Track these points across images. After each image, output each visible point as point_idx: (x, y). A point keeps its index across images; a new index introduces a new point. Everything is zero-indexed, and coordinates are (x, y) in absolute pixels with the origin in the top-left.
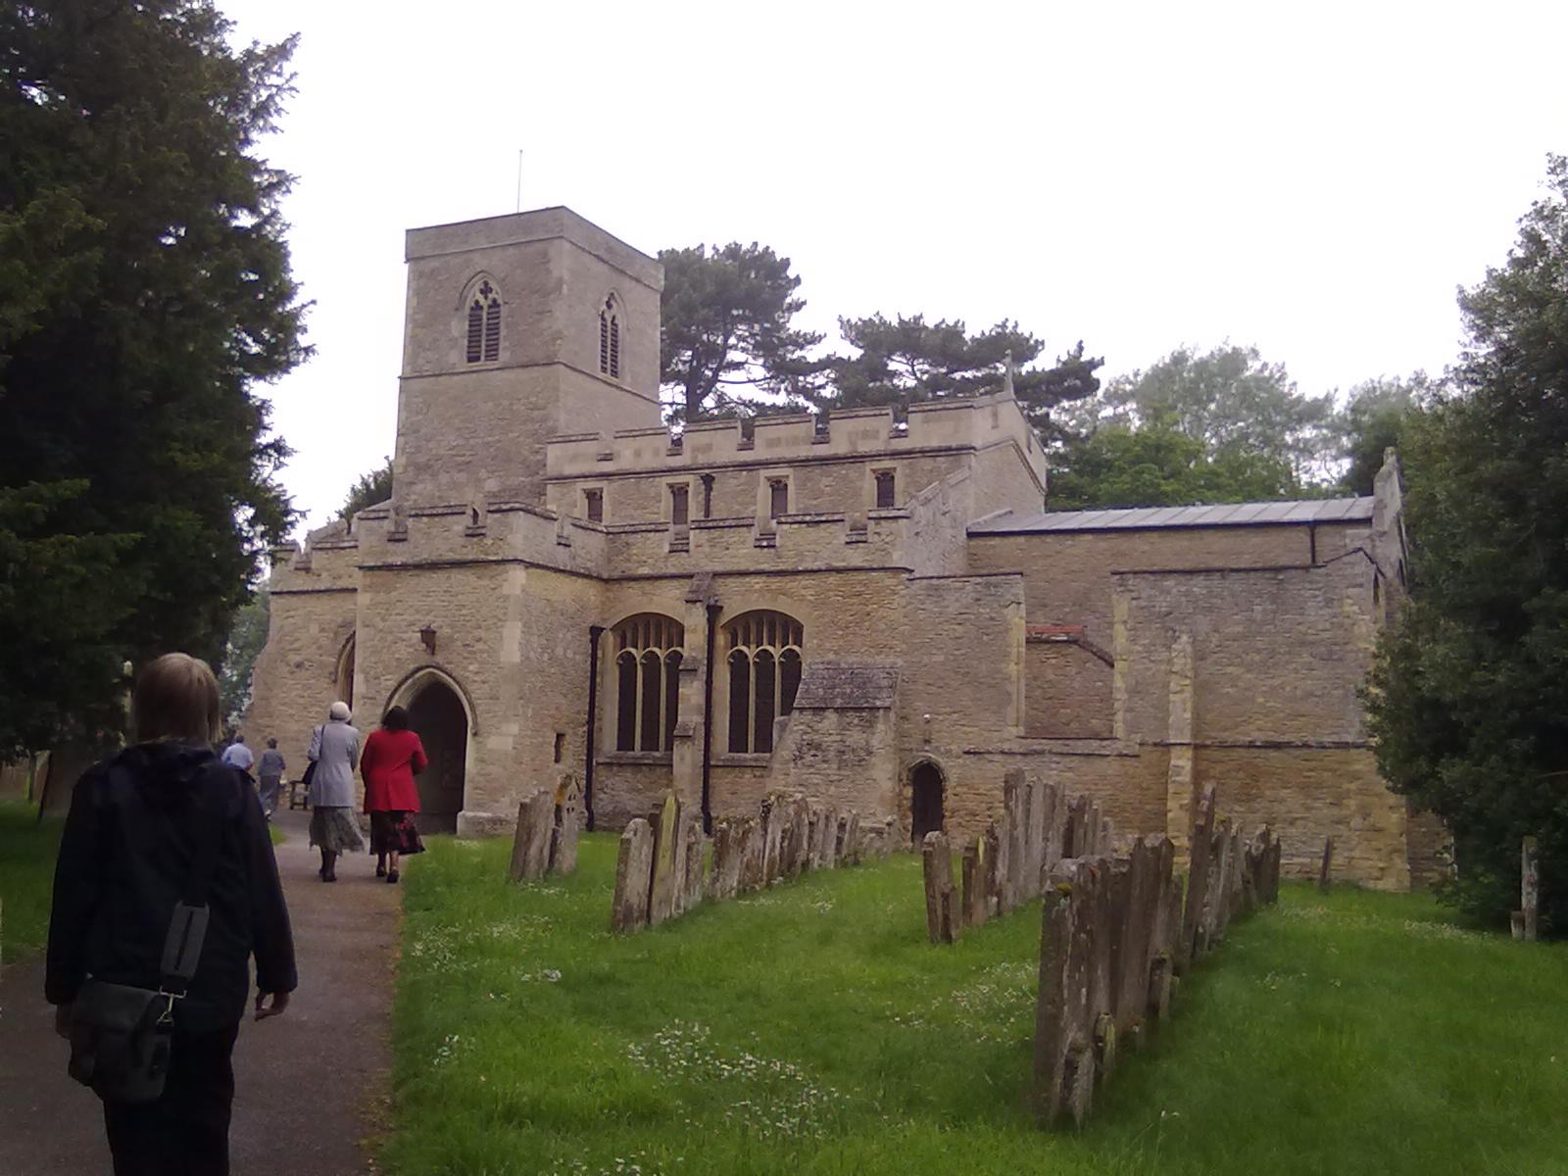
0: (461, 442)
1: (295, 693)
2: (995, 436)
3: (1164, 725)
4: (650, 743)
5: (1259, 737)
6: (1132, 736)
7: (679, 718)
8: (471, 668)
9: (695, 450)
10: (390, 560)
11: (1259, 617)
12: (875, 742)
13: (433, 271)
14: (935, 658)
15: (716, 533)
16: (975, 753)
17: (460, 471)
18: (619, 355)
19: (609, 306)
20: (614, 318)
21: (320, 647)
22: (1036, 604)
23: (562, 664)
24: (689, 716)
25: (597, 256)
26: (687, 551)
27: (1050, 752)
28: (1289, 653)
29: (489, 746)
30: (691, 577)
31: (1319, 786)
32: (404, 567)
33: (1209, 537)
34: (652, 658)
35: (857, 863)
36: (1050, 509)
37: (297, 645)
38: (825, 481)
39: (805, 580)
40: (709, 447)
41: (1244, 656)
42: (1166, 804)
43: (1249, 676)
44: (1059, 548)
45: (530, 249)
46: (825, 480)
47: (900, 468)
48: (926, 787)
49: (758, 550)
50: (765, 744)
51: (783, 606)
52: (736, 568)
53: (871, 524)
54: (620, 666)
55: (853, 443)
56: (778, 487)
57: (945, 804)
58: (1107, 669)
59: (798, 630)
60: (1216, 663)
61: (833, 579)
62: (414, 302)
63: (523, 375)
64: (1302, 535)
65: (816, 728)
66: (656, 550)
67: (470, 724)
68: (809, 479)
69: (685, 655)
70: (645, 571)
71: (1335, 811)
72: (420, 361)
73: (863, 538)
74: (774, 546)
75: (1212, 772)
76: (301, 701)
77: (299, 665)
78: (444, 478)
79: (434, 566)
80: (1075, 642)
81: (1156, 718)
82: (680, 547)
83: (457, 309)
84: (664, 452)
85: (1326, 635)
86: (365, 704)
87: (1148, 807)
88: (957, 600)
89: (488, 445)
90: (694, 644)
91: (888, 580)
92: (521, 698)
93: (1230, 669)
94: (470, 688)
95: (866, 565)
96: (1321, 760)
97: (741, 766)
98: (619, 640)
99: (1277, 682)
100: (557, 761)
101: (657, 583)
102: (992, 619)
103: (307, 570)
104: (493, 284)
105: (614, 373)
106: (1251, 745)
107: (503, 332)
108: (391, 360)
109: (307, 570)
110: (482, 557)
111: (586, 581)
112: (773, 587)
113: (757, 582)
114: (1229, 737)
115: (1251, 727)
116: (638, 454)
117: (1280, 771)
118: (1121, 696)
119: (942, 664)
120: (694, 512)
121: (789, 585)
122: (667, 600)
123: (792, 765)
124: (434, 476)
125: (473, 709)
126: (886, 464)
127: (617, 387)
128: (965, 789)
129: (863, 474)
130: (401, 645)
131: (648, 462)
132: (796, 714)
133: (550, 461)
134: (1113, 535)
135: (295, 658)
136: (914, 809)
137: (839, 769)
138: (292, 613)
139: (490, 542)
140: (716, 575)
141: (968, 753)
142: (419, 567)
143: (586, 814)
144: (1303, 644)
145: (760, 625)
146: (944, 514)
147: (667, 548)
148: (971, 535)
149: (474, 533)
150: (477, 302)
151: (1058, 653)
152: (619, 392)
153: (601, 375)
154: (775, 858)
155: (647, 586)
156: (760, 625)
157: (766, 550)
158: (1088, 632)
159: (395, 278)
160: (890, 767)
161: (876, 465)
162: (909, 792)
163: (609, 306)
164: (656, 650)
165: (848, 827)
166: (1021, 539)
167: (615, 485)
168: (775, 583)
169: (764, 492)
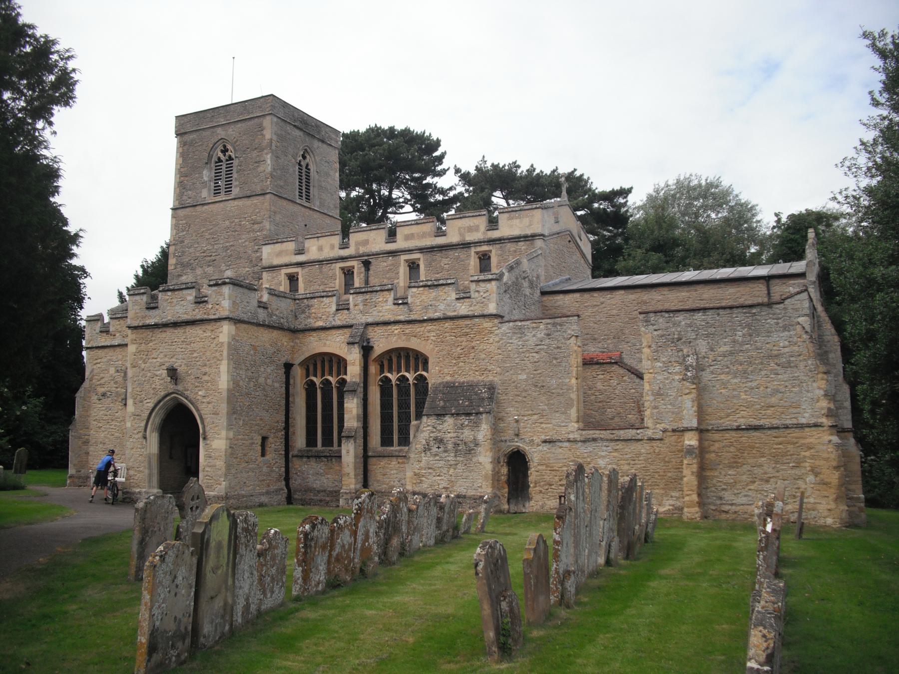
0: (209, 247)
1: (102, 413)
2: (556, 228)
3: (678, 415)
4: (328, 441)
5: (742, 422)
6: (658, 426)
7: (345, 425)
8: (200, 393)
9: (358, 244)
10: (148, 322)
11: (740, 339)
12: (480, 437)
13: (192, 141)
14: (520, 377)
15: (368, 296)
16: (550, 442)
17: (209, 266)
18: (311, 188)
19: (304, 157)
20: (307, 165)
21: (116, 383)
22: (588, 337)
23: (264, 389)
24: (352, 420)
25: (295, 126)
26: (348, 309)
27: (602, 439)
28: (762, 363)
29: (213, 447)
30: (351, 326)
31: (785, 454)
32: (156, 326)
33: (701, 289)
34: (327, 383)
35: (455, 537)
36: (593, 277)
37: (102, 381)
38: (445, 261)
39: (430, 326)
40: (366, 242)
41: (731, 366)
42: (682, 472)
43: (735, 381)
44: (602, 300)
45: (252, 122)
46: (444, 260)
47: (495, 253)
48: (516, 465)
49: (396, 306)
50: (405, 440)
51: (414, 344)
52: (382, 319)
53: (473, 286)
54: (306, 389)
55: (461, 234)
56: (413, 267)
57: (530, 479)
58: (637, 380)
59: (426, 361)
60: (712, 373)
61: (448, 325)
62: (181, 161)
63: (247, 202)
64: (761, 286)
65: (438, 428)
66: (327, 310)
67: (201, 431)
68: (434, 261)
69: (348, 380)
70: (320, 324)
71: (797, 472)
72: (185, 198)
73: (468, 295)
74: (406, 303)
75: (712, 448)
76: (105, 418)
77: (104, 395)
78: (199, 271)
79: (176, 325)
80: (616, 363)
81: (673, 413)
82: (343, 307)
83: (207, 163)
84: (337, 246)
85: (787, 350)
86: (134, 419)
87: (669, 474)
88: (534, 336)
89: (227, 248)
90: (353, 372)
91: (487, 324)
92: (234, 413)
93: (722, 377)
94: (201, 407)
95: (470, 313)
96: (786, 437)
97: (390, 456)
98: (304, 371)
99: (754, 384)
100: (263, 455)
101: (328, 332)
102: (558, 348)
103: (107, 332)
104: (229, 147)
105: (308, 199)
106: (738, 429)
107: (235, 175)
108: (168, 199)
109: (107, 332)
110: (206, 317)
111: (279, 332)
112: (407, 331)
113: (396, 329)
114: (727, 423)
115: (738, 416)
116: (320, 249)
117: (757, 445)
118: (648, 400)
119: (526, 381)
120: (358, 282)
121: (418, 330)
122: (335, 344)
123: (423, 455)
124: (193, 269)
125: (203, 423)
126: (485, 248)
127: (310, 208)
128: (544, 468)
129: (469, 256)
130: (156, 379)
131: (328, 253)
132: (424, 419)
133: (264, 256)
134: (639, 290)
135: (101, 390)
136: (509, 482)
137: (456, 456)
138: (99, 361)
139: (210, 306)
140: (368, 325)
141: (545, 442)
142: (166, 325)
143: (286, 491)
144: (771, 357)
145: (399, 357)
146: (524, 278)
147: (334, 308)
148: (544, 293)
149: (200, 301)
150: (219, 158)
151: (605, 371)
152: (311, 212)
153: (298, 201)
154: (370, 548)
155: (322, 334)
156: (399, 357)
157: (401, 306)
158: (624, 356)
159: (167, 148)
160: (491, 454)
161: (479, 249)
162: (505, 470)
163: (304, 157)
164: (330, 378)
165: (446, 509)
166: (577, 295)
167: (306, 270)
168: (408, 329)
169: (403, 270)
